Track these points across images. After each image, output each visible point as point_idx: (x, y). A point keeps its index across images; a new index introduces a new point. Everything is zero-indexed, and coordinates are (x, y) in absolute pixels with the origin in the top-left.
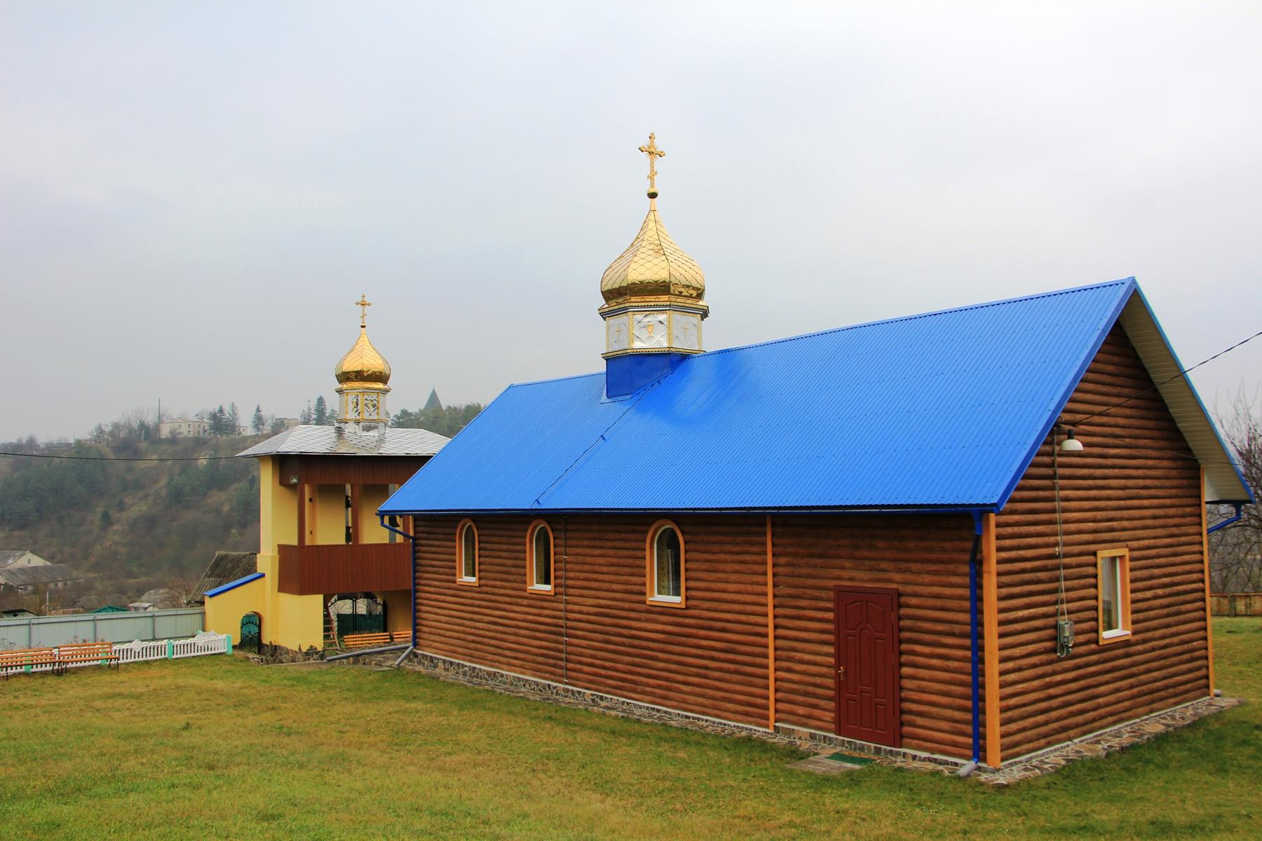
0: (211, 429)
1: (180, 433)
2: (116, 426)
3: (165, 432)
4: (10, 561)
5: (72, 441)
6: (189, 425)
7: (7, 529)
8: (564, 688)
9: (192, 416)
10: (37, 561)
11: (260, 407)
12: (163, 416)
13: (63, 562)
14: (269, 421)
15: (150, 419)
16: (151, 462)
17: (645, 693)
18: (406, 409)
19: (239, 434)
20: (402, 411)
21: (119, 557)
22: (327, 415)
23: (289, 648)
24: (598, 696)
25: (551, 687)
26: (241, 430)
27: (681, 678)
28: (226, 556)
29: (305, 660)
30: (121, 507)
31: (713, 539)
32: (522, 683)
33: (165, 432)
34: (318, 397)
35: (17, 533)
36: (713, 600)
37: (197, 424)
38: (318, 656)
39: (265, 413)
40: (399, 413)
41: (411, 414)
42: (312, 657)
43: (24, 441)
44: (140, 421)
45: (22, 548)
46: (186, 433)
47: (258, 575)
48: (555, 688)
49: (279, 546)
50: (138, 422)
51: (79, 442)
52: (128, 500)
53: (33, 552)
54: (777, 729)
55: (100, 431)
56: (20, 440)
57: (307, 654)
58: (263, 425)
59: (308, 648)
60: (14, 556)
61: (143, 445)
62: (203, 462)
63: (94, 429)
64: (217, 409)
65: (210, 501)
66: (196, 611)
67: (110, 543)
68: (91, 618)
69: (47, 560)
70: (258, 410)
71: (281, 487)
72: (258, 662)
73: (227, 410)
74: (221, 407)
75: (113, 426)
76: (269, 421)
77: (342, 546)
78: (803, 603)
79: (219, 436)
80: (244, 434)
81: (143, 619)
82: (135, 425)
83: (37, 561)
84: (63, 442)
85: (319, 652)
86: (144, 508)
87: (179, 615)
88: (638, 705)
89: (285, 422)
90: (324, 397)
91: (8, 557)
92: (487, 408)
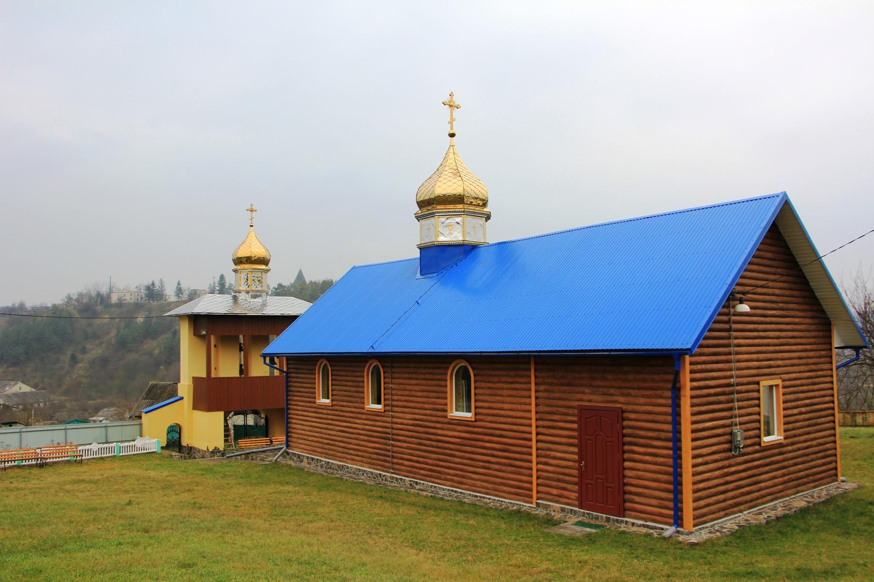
0: (146, 297)
1: (125, 300)
2: (81, 295)
3: (114, 299)
4: (7, 388)
5: (50, 305)
6: (131, 294)
7: (5, 366)
8: (390, 476)
9: (133, 288)
10: (26, 388)
11: (180, 282)
12: (113, 288)
13: (43, 389)
14: (187, 291)
15: (104, 290)
16: (105, 319)
17: (446, 480)
18: (281, 283)
19: (166, 300)
20: (278, 285)
21: (82, 385)
22: (226, 287)
23: (200, 448)
24: (414, 482)
25: (382, 476)
26: (167, 297)
27: (471, 469)
28: (156, 385)
29: (211, 457)
30: (84, 351)
31: (493, 373)
32: (361, 473)
33: (114, 299)
34: (220, 274)
35: (11, 369)
36: (493, 415)
37: (136, 293)
38: (220, 454)
39: (184, 286)
40: (276, 286)
41: (285, 287)
42: (216, 454)
43: (17, 305)
44: (97, 292)
45: (15, 379)
46: (129, 300)
47: (179, 398)
48: (384, 476)
49: (193, 378)
50: (96, 292)
51: (54, 306)
52: (89, 346)
53: (23, 382)
54: (538, 505)
55: (69, 298)
56: (14, 305)
57: (212, 452)
58: (182, 294)
59: (213, 448)
60: (10, 385)
61: (99, 308)
62: (140, 320)
63: (65, 297)
64: (150, 283)
65: (145, 347)
66: (136, 423)
67: (76, 376)
68: (63, 428)
69: (32, 387)
70: (179, 284)
71: (194, 337)
72: (179, 458)
73: (157, 284)
74: (153, 281)
75: (78, 295)
76: (187, 291)
77: (237, 378)
78: (556, 417)
79: (151, 302)
80: (169, 300)
81: (99, 428)
82: (94, 294)
83: (26, 388)
84: (44, 306)
85: (221, 451)
86: (100, 352)
87: (124, 425)
88: (442, 488)
89: (197, 292)
90: (225, 275)
91: (6, 385)
92: (337, 282)
